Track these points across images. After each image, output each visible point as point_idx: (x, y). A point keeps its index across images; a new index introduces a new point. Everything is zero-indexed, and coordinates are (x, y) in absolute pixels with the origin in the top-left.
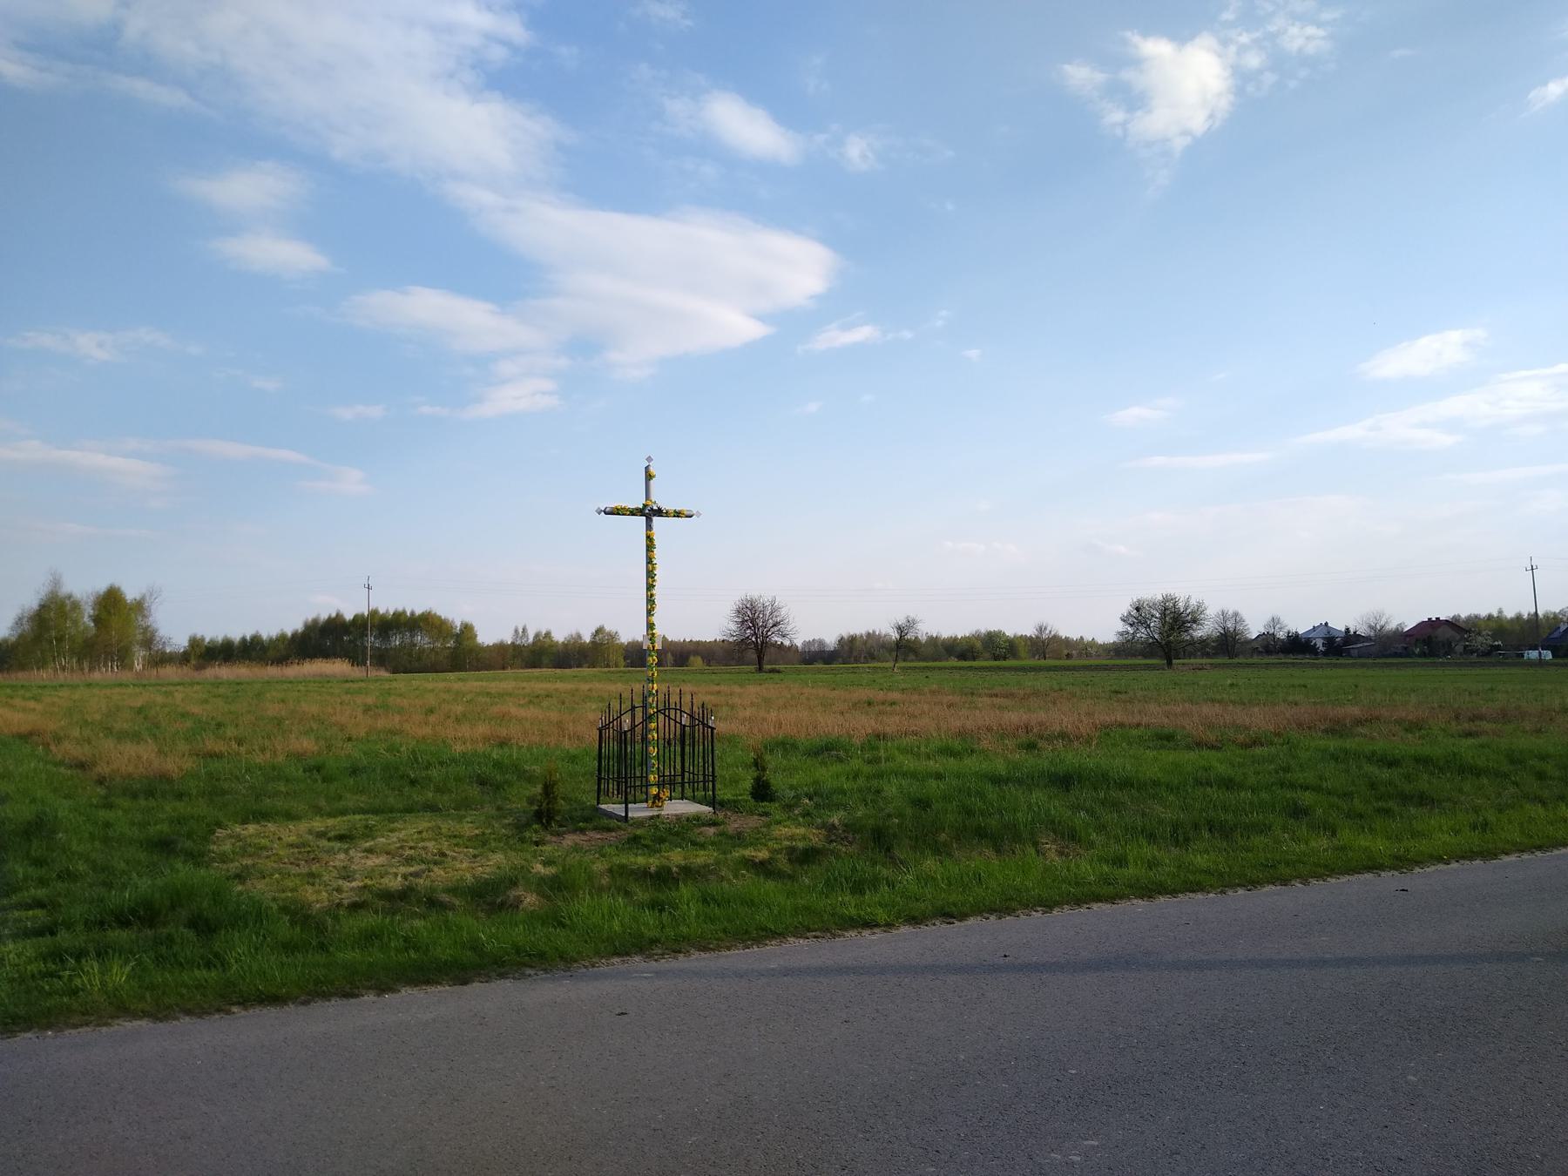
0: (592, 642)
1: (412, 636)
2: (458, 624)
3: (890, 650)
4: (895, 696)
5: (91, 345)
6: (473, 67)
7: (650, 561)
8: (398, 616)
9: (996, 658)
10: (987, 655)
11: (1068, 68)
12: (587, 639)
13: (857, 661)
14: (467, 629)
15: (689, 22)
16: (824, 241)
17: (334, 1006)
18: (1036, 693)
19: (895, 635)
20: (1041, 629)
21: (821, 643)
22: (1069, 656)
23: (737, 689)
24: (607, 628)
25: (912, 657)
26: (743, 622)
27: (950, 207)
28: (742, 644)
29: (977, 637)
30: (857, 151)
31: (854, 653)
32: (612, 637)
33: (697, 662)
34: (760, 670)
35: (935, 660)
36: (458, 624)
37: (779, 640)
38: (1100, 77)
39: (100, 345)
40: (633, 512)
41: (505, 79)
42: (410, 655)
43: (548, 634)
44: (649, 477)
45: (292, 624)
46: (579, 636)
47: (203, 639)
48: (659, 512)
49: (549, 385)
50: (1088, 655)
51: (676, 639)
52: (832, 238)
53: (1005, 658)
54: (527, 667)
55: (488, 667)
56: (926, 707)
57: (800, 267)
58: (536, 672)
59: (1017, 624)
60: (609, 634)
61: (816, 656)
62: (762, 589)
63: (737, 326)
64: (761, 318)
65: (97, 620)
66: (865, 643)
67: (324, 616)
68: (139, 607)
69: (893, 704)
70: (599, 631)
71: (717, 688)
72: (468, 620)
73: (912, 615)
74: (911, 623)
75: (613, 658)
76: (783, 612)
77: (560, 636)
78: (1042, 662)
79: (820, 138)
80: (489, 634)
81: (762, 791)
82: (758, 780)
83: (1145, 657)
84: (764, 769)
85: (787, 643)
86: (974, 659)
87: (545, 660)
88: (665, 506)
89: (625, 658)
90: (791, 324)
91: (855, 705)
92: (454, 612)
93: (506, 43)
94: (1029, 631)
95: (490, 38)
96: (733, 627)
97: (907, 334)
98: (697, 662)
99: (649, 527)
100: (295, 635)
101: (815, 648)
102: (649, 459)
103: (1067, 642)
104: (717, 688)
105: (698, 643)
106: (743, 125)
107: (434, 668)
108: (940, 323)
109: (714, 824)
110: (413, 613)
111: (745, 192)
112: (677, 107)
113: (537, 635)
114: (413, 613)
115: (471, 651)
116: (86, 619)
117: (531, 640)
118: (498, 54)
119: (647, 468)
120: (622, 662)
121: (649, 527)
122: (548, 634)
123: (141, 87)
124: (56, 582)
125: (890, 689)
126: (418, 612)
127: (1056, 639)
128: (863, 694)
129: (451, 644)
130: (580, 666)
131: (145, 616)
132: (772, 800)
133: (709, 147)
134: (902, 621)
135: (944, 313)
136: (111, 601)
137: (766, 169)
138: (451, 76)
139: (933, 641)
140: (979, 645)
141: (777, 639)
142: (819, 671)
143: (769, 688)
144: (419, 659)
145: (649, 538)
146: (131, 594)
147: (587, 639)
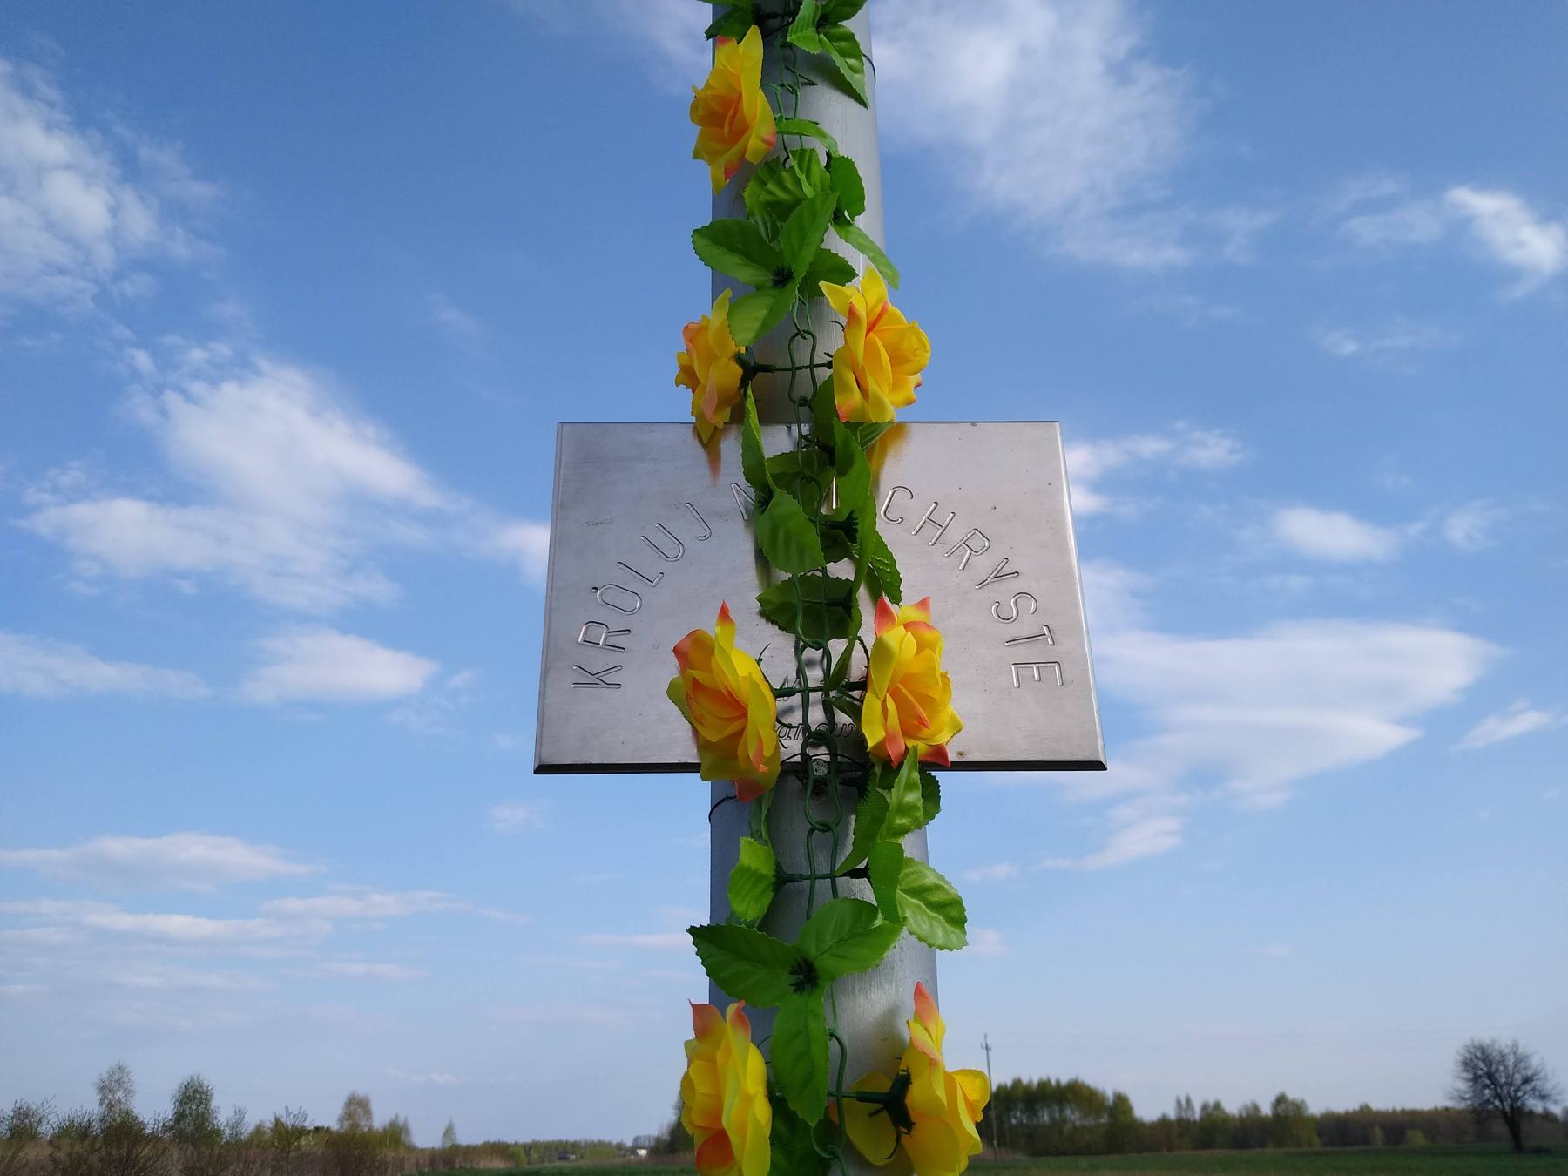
0: (1276, 1116)
1: (1061, 1111)
2: (1110, 1095)
8: (1044, 1085)
12: (1266, 1110)
14: (1121, 1101)
16: (1459, 629)
28: (1478, 1116)
30: (1463, 528)
32: (1298, 1107)
33: (1417, 1139)
36: (1110, 1095)
46: (1256, 1108)
47: (1049, 1081)
52: (1465, 624)
54: (1196, 1148)
57: (1440, 660)
58: (1206, 1154)
62: (1498, 1030)
63: (1373, 733)
64: (1403, 721)
70: (1281, 1100)
77: (1233, 1106)
79: (1415, 529)
80: (1149, 1108)
83: (795, 617)
89: (1320, 1134)
90: (1442, 724)
92: (1105, 1080)
96: (1462, 1086)
110: (1058, 1083)
111: (1340, 596)
113: (1205, 1107)
114: (1058, 1083)
117: (1197, 1115)
120: (1316, 1140)
122: (1217, 1106)
126: (1064, 1080)
129: (1104, 1119)
130: (1263, 1145)
133: (1291, 561)
141: (1537, 1106)
147: (1266, 1110)
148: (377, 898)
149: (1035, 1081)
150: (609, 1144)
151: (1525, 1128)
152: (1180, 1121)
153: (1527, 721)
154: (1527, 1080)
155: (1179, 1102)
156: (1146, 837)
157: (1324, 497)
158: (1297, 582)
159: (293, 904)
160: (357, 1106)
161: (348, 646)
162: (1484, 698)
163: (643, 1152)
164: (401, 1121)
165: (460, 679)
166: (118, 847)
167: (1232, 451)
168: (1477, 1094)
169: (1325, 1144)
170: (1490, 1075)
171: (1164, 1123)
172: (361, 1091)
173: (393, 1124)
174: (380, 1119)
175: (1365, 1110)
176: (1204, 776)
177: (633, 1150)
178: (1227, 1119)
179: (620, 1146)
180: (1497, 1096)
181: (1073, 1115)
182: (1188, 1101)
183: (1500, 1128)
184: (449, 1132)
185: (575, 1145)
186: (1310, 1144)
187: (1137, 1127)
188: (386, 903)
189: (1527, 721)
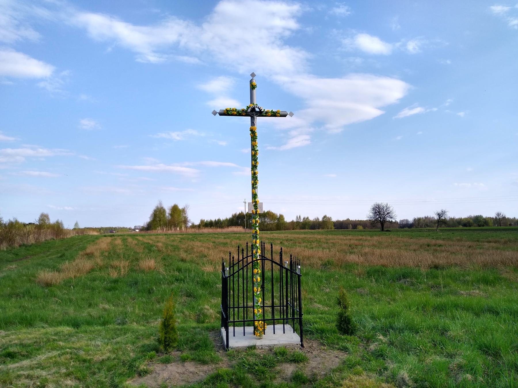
3: (435, 223)
4: (440, 242)
5: (175, 136)
6: (280, 39)
7: (253, 148)
9: (479, 226)
10: (476, 225)
11: (493, 8)
12: (321, 219)
13: (421, 227)
15: (349, 13)
16: (403, 79)
17: (458, 211)
18: (510, 241)
19: (436, 217)
20: (498, 214)
21: (407, 221)
22: (510, 225)
23: (369, 238)
24: (328, 216)
25: (443, 226)
26: (375, 213)
27: (449, 62)
29: (470, 218)
31: (420, 226)
32: (329, 219)
33: (360, 228)
34: (383, 230)
35: (453, 227)
37: (391, 220)
38: (506, 9)
39: (178, 136)
40: (240, 114)
41: (289, 41)
42: (264, 225)
43: (308, 218)
44: (253, 87)
45: (229, 216)
46: (318, 219)
48: (261, 114)
49: (308, 137)
50: (510, 225)
51: (353, 220)
52: (404, 78)
53: (483, 226)
55: (288, 229)
56: (458, 248)
57: (394, 89)
59: (489, 212)
60: (328, 218)
61: (405, 226)
62: (382, 201)
63: (371, 112)
64: (380, 108)
65: (171, 215)
66: (424, 220)
67: (238, 213)
68: (183, 210)
69: (440, 246)
70: (325, 217)
71: (361, 237)
72: (282, 214)
73: (444, 209)
74: (443, 213)
75: (330, 226)
76: (391, 209)
77: (312, 218)
78: (499, 227)
79: (398, 44)
80: (288, 219)
81: (345, 326)
82: (341, 315)
84: (345, 307)
85: (394, 221)
86: (470, 226)
87: (307, 227)
88: (265, 108)
89: (334, 226)
90: (391, 110)
91: (421, 246)
93: (290, 30)
94: (493, 215)
95: (285, 29)
96: (372, 215)
97: (435, 109)
98: (360, 228)
99: (253, 123)
100: (230, 219)
101: (405, 223)
102: (253, 75)
103: (509, 219)
104: (361, 237)
105: (361, 221)
106: (370, 44)
107: (271, 229)
108: (447, 104)
109: (296, 360)
111: (373, 66)
112: (346, 41)
113: (304, 219)
115: (283, 224)
116: (167, 215)
118: (287, 33)
119: (251, 81)
120: (333, 227)
121: (253, 123)
122: (308, 218)
123: (185, 59)
124: (160, 204)
125: (437, 239)
127: (504, 218)
128: (424, 241)
131: (185, 214)
132: (352, 333)
133: (358, 53)
134: (440, 211)
135: (449, 100)
136: (175, 209)
137: (379, 57)
138: (273, 43)
139: (452, 220)
140: (471, 221)
141: (388, 219)
142: (406, 231)
143: (384, 238)
144: (267, 226)
145: (253, 132)
146: (181, 207)
147: (321, 219)
148: (41, 150)
149: (146, 224)
150: (126, 228)
151: (385, 226)
152: (297, 222)
153: (417, 110)
154: (388, 213)
155: (297, 217)
156: (299, 141)
157: (373, 30)
158: (358, 60)
159: (9, 151)
160: (44, 218)
161: (19, 57)
162: (406, 102)
163: (137, 230)
164: (60, 221)
165: (65, 73)
166: (164, 135)
167: (347, 11)
168: (375, 216)
169: (336, 229)
170: (379, 212)
171: (293, 222)
172: (45, 212)
173: (57, 222)
174: (52, 220)
175: (348, 220)
176: (319, 123)
177: (134, 230)
178: (310, 222)
179: (130, 229)
180: (380, 217)
181: (267, 220)
182: (300, 217)
183: (379, 225)
184: (76, 224)
185: (115, 228)
186: (331, 229)
187: (285, 223)
188: (43, 152)
189: (417, 110)
